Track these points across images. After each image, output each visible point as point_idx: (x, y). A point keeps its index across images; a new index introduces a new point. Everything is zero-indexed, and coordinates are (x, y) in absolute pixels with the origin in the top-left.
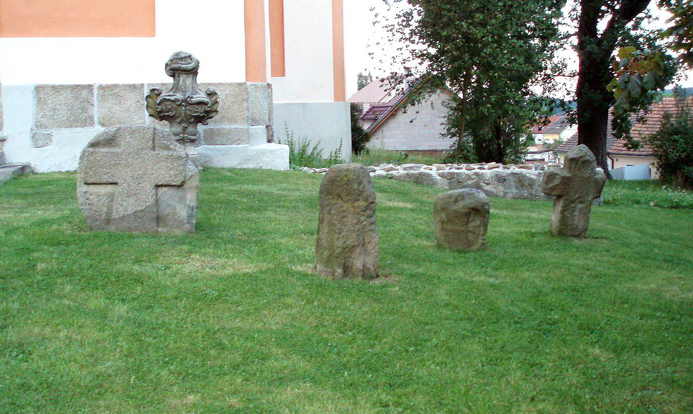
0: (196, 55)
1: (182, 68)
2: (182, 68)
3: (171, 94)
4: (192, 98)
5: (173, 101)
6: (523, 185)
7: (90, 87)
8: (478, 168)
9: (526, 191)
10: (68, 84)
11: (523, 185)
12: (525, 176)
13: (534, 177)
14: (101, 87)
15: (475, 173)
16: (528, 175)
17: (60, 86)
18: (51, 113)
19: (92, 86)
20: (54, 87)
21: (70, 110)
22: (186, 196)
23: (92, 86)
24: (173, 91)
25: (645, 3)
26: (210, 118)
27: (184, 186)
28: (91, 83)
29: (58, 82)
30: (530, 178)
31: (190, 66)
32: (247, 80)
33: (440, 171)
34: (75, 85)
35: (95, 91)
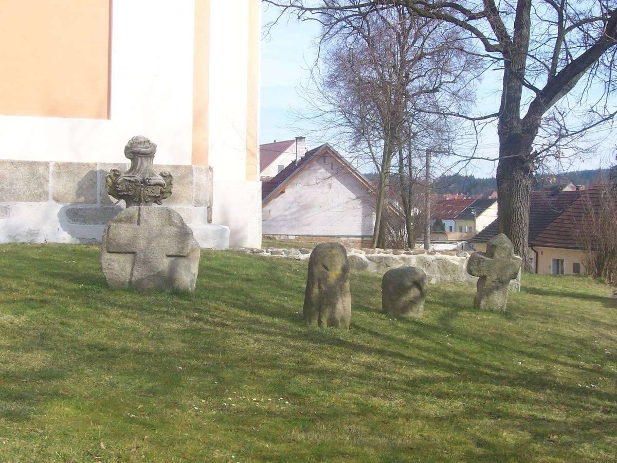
0: (153, 140)
1: (138, 152)
2: (138, 152)
3: (130, 175)
4: (150, 179)
5: (133, 182)
6: (446, 271)
7: (47, 164)
8: (404, 253)
9: (449, 277)
10: (26, 160)
11: (446, 271)
12: (449, 262)
13: (456, 263)
14: (58, 165)
15: (402, 258)
16: (451, 261)
17: (18, 162)
18: (8, 187)
19: (49, 163)
20: (12, 163)
21: (26, 184)
22: (190, 265)
23: (49, 163)
24: (132, 173)
25: (519, 5)
26: (165, 198)
27: (188, 257)
28: (48, 160)
29: (16, 158)
30: (454, 264)
31: (148, 150)
32: (192, 163)
33: (369, 255)
34: (33, 162)
35: (52, 168)
